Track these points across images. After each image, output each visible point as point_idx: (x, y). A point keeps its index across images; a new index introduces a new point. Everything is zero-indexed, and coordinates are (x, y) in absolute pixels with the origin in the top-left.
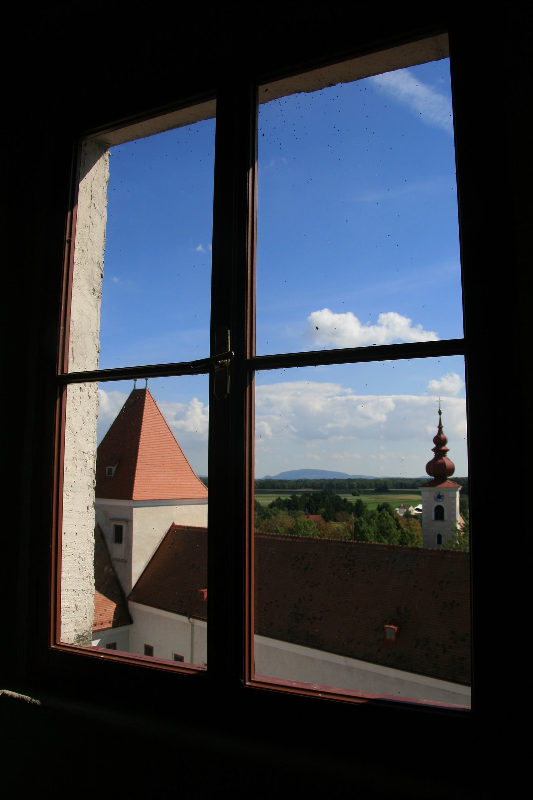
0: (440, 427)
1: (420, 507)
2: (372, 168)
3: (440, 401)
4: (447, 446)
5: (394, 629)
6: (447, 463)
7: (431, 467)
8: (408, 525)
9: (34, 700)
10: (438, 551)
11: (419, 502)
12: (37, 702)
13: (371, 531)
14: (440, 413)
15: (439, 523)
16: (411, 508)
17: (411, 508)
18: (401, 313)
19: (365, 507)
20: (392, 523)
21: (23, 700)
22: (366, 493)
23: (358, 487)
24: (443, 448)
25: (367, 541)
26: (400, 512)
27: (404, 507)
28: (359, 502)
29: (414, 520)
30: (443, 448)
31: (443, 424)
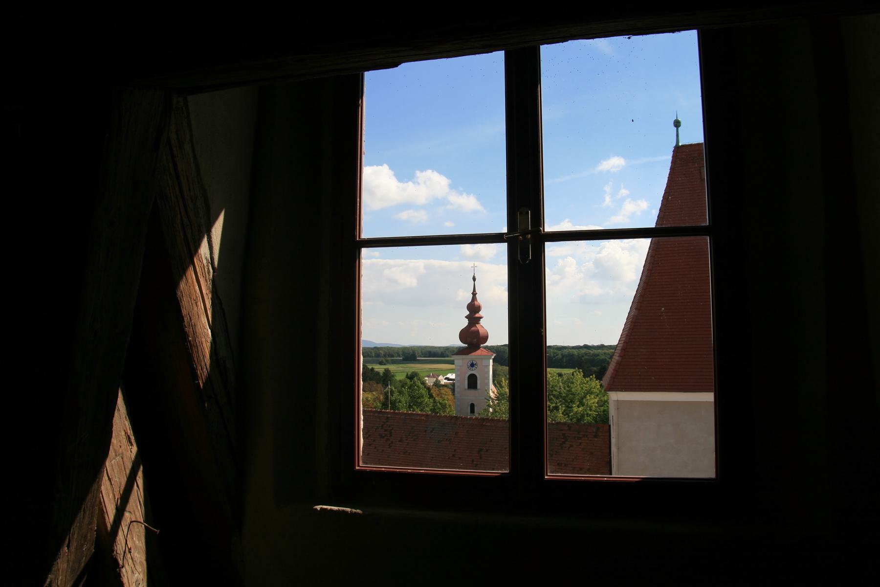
0: (474, 294)
1: (452, 376)
2: (630, 116)
3: (474, 267)
4: (481, 313)
5: (560, 466)
6: (481, 331)
7: (464, 335)
8: (439, 394)
9: (354, 510)
10: (471, 419)
11: (451, 371)
12: (358, 511)
13: (403, 403)
14: (474, 279)
15: (472, 392)
16: (441, 378)
17: (441, 378)
18: (440, 172)
19: (393, 376)
20: (423, 391)
21: (343, 511)
22: (394, 362)
23: (385, 356)
24: (477, 315)
25: (398, 409)
26: (430, 382)
27: (434, 376)
28: (387, 371)
29: (446, 389)
30: (477, 315)
31: (477, 291)
